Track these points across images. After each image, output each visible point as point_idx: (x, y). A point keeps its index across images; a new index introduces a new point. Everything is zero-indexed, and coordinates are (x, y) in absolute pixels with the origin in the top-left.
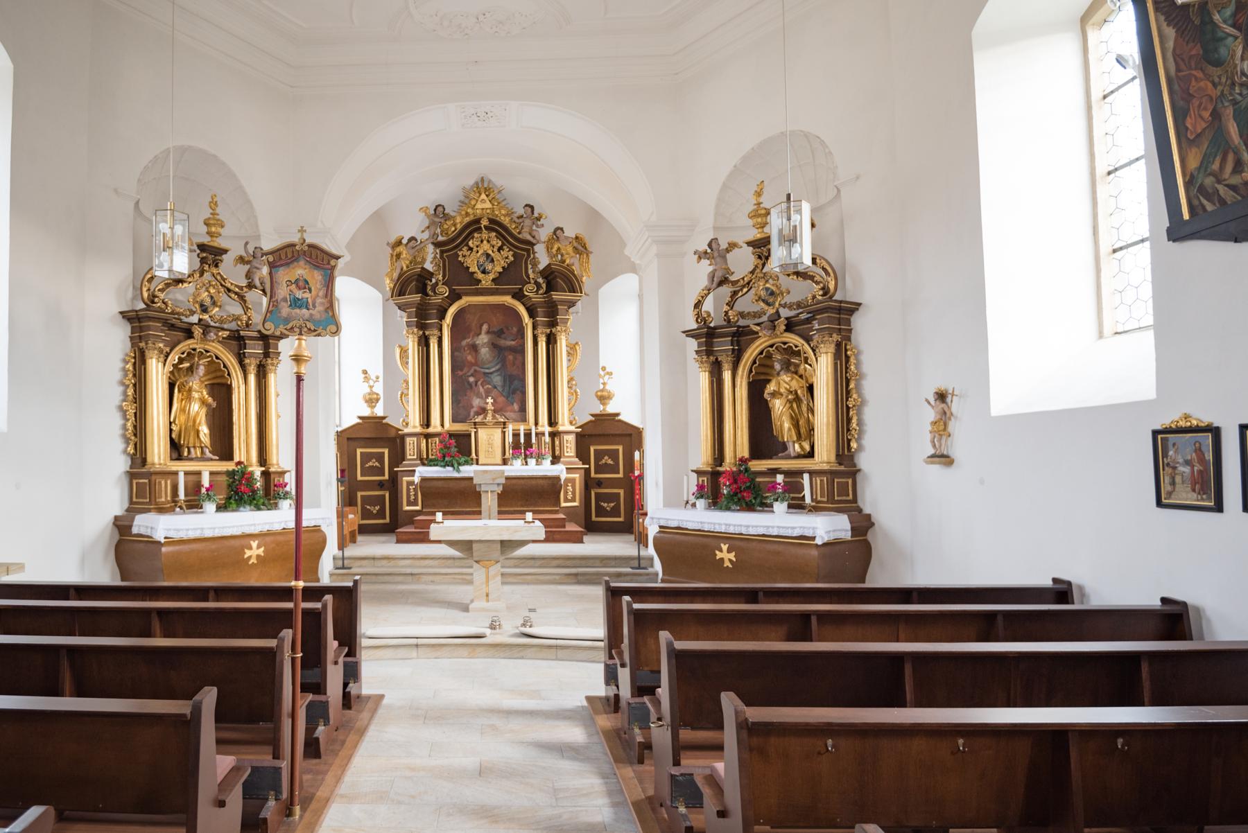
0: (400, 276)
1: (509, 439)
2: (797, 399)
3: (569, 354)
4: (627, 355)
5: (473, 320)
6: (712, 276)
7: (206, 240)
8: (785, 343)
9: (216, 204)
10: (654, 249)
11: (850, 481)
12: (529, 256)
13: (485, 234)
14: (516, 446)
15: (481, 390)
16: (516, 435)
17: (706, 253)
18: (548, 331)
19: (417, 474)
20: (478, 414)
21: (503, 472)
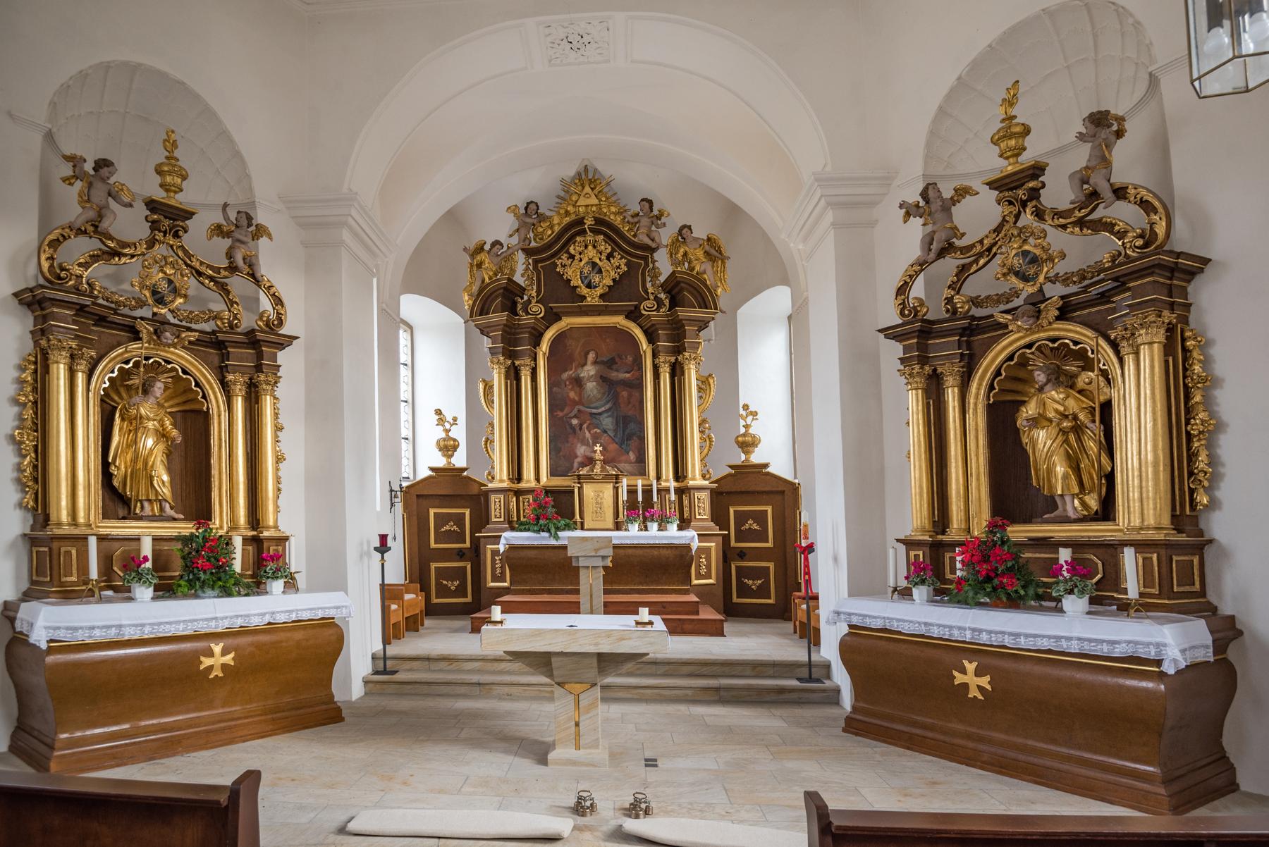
0: (481, 290)
1: (624, 496)
2: (1078, 429)
3: (700, 389)
4: (783, 388)
5: (575, 347)
6: (928, 241)
7: (159, 195)
8: (1054, 340)
9: (175, 144)
10: (829, 217)
11: (1196, 560)
12: (647, 265)
13: (590, 237)
14: (632, 506)
15: (587, 434)
16: (632, 492)
17: (917, 206)
18: (673, 359)
19: (503, 541)
20: (583, 465)
21: (610, 539)
